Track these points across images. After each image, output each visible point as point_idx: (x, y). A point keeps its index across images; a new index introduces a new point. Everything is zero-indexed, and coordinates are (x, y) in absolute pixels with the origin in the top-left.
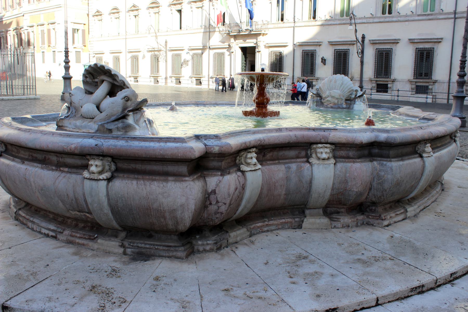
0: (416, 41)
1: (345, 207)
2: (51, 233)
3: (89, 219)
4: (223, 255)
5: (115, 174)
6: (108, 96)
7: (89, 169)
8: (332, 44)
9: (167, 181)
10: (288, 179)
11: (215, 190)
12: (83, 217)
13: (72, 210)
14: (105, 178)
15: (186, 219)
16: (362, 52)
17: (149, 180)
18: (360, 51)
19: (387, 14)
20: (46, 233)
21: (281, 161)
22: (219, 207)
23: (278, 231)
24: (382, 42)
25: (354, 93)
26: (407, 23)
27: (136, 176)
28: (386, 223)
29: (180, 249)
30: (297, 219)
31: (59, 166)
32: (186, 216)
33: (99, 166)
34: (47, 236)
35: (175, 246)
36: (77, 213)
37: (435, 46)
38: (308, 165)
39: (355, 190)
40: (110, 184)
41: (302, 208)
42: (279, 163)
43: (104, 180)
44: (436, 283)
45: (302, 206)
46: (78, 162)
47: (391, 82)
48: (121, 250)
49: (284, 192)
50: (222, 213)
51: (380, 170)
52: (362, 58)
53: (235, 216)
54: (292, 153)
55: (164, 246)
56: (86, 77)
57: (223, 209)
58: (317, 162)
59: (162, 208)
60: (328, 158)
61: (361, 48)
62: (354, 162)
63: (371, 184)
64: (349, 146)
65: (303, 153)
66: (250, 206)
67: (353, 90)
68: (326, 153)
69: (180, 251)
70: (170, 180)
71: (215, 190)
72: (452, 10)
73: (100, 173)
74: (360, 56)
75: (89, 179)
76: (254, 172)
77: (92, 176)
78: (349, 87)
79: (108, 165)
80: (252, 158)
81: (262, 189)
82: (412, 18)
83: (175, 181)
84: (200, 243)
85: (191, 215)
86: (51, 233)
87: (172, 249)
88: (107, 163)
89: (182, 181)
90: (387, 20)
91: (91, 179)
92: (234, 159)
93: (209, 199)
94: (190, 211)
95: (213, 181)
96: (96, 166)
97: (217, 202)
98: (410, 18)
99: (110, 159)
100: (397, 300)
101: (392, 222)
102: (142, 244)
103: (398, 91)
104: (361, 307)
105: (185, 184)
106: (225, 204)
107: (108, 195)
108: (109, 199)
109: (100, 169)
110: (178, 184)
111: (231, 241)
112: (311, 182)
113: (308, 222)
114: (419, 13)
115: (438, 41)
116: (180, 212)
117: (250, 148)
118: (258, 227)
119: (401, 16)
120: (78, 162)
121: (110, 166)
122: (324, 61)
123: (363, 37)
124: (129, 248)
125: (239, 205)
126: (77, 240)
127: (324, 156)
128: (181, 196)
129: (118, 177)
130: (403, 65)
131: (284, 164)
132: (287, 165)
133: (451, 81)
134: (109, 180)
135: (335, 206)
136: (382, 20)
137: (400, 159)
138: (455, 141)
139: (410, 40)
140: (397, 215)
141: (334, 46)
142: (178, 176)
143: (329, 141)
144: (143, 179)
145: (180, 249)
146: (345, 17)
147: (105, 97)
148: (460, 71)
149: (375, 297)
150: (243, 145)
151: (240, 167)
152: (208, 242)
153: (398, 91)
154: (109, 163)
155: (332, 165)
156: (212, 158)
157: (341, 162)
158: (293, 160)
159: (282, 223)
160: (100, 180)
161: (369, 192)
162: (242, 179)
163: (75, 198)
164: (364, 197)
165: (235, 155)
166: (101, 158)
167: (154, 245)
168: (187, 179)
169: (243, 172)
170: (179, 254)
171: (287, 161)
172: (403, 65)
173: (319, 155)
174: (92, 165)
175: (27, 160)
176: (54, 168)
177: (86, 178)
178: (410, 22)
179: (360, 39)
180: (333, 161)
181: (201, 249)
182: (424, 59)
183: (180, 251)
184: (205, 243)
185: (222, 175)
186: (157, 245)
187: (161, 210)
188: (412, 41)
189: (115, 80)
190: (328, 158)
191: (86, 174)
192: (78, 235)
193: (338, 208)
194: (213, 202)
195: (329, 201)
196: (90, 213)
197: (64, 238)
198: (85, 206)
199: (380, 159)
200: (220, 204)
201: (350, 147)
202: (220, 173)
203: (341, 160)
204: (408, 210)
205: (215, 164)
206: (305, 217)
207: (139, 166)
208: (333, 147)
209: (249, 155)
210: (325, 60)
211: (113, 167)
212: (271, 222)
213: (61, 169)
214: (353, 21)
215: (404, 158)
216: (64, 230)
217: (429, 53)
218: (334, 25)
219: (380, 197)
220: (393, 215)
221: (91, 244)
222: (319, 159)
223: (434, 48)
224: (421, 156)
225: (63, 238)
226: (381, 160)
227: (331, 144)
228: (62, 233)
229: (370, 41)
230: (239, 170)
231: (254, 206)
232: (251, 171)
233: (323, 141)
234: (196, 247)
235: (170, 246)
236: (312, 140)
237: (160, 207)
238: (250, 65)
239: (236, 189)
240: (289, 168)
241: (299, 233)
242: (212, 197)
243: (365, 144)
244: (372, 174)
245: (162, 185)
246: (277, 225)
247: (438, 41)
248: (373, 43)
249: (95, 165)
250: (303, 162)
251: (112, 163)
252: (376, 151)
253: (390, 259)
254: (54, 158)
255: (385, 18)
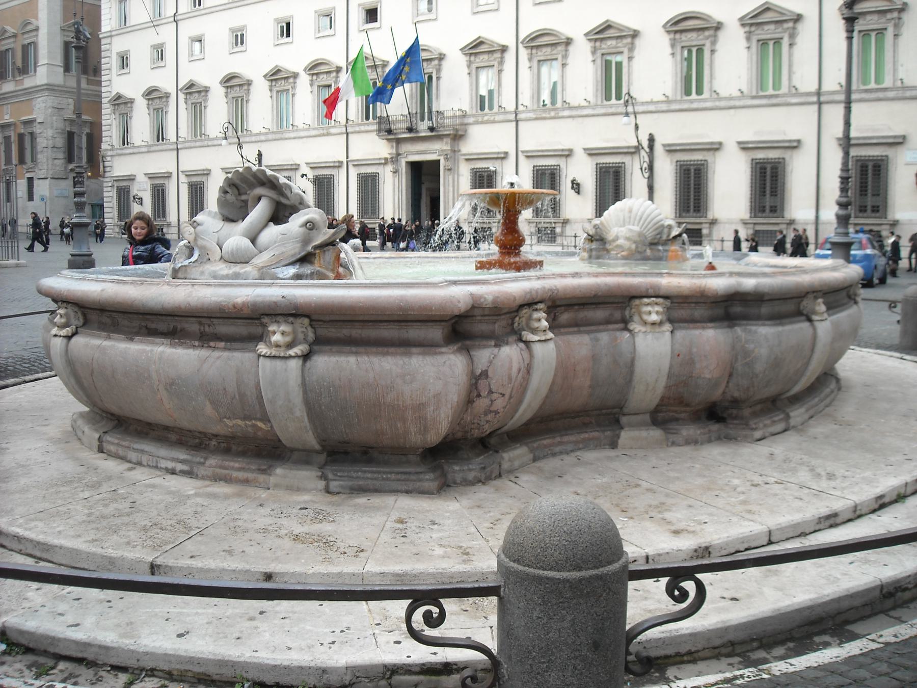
0: (750, 146)
1: (688, 409)
2: (180, 467)
3: (259, 433)
4: (497, 490)
5: (316, 348)
6: (272, 224)
7: (270, 342)
8: (592, 153)
9: (409, 354)
10: (595, 358)
11: (487, 371)
12: (250, 429)
13: (229, 418)
14: (299, 353)
15: (441, 423)
16: (651, 168)
17: (377, 354)
18: (645, 165)
19: (694, 96)
20: (170, 467)
21: (582, 329)
22: (492, 401)
23: (578, 453)
24: (688, 147)
25: (666, 230)
26: (732, 111)
27: (354, 349)
28: (758, 434)
29: (427, 477)
30: (608, 433)
31: (206, 339)
32: (443, 415)
33: (288, 335)
34: (173, 472)
35: (417, 473)
36: (240, 422)
37: (787, 155)
38: (627, 335)
39: (708, 376)
40: (308, 364)
41: (615, 414)
42: (579, 332)
43: (297, 356)
44: (855, 511)
45: (615, 410)
46: (240, 329)
47: (707, 225)
48: (321, 484)
49: (588, 383)
50: (497, 412)
51: (747, 342)
52: (651, 179)
53: (512, 422)
54: (600, 314)
55: (398, 473)
56: (226, 192)
57: (499, 404)
58: (643, 329)
59: (401, 403)
60: (661, 323)
61: (647, 159)
62: (704, 328)
63: (732, 367)
64: (694, 300)
65: (617, 315)
66: (536, 405)
67: (663, 226)
68: (657, 313)
69: (427, 480)
70: (414, 354)
71: (487, 371)
72: (813, 87)
73: (290, 346)
74: (646, 175)
75: (269, 357)
76: (544, 344)
77: (274, 352)
78: (655, 220)
79: (303, 332)
80: (539, 320)
81: (555, 375)
82: (741, 103)
83: (424, 354)
84: (457, 468)
85: (450, 413)
86: (180, 467)
87: (413, 477)
88: (300, 330)
89: (436, 354)
90: (695, 105)
91: (274, 357)
92: (510, 321)
93: (476, 388)
94: (449, 406)
95: (484, 356)
96: (283, 333)
97: (491, 392)
98: (737, 103)
99: (306, 321)
100: (799, 536)
101: (767, 434)
102: (357, 472)
103: (723, 241)
104: (746, 546)
105: (440, 359)
106: (503, 395)
107: (304, 384)
108: (305, 392)
109: (288, 339)
110: (429, 359)
111: (506, 466)
112: (633, 360)
113: (626, 436)
114: (754, 93)
115: (795, 146)
116: (432, 408)
117: (536, 303)
118: (546, 447)
119: (720, 99)
120: (240, 329)
121: (306, 335)
122: (576, 187)
123: (651, 140)
124: (335, 480)
125: (520, 402)
126: (235, 474)
127: (654, 317)
128: (434, 379)
129: (320, 352)
130: (730, 194)
131: (588, 332)
132: (592, 335)
133: (820, 222)
134: (306, 357)
135: (672, 408)
136: (685, 106)
137: (778, 322)
138: (856, 303)
139: (739, 143)
140: (774, 422)
141: (594, 157)
142: (427, 346)
143: (661, 293)
144: (367, 354)
145: (427, 477)
146: (614, 101)
147: (266, 226)
148: (840, 197)
149: (764, 528)
150: (528, 296)
151: (520, 335)
152: (471, 466)
153: (723, 241)
154: (304, 330)
155: (668, 334)
156: (479, 318)
157: (681, 328)
158: (601, 327)
159: (584, 440)
160: (290, 357)
161: (728, 382)
162: (526, 355)
163: (239, 394)
164: (720, 391)
165: (513, 314)
166: (291, 319)
167: (379, 472)
168: (444, 350)
169: (527, 343)
170: (427, 485)
171: (593, 328)
172: (730, 194)
173: (645, 317)
174: (274, 333)
175: (138, 334)
176: (197, 343)
177: (264, 356)
178: (739, 111)
179: (645, 144)
180: (667, 327)
181: (458, 477)
182: (768, 182)
183: (427, 480)
184: (466, 468)
185: (496, 346)
186: (384, 473)
187: (399, 405)
188: (744, 147)
189: (282, 194)
190: (661, 323)
191: (262, 349)
192: (237, 465)
193: (676, 412)
194: (484, 393)
195: (662, 399)
196: (265, 419)
197: (209, 472)
198: (257, 407)
199: (744, 322)
200: (495, 396)
201: (696, 303)
202: (493, 343)
203: (681, 325)
204: (792, 414)
205: (484, 327)
206: (622, 428)
207: (356, 332)
208: (668, 303)
209: (536, 315)
210: (578, 185)
211: (311, 336)
212: (566, 439)
213: (212, 344)
214: (630, 109)
215: (784, 321)
216: (206, 459)
217: (777, 168)
218: (593, 116)
219: (748, 388)
220: (768, 422)
221: (262, 478)
222: (645, 323)
223: (784, 159)
224: (810, 320)
225: (204, 473)
226: (747, 325)
227: (666, 297)
228: (203, 464)
229: (664, 145)
230: (520, 340)
231: (541, 408)
232: (539, 341)
233: (651, 292)
234: (450, 476)
235: (410, 473)
236: (634, 294)
237: (398, 400)
238: (429, 199)
239: (519, 370)
240: (597, 340)
241: (612, 453)
242: (482, 383)
243: (723, 296)
244: (733, 348)
245: (401, 362)
246: (576, 442)
247: (795, 146)
248: (671, 150)
249: (278, 333)
250: (618, 330)
251: (309, 329)
252: (737, 309)
253: (776, 482)
254: (193, 326)
255: (692, 101)
